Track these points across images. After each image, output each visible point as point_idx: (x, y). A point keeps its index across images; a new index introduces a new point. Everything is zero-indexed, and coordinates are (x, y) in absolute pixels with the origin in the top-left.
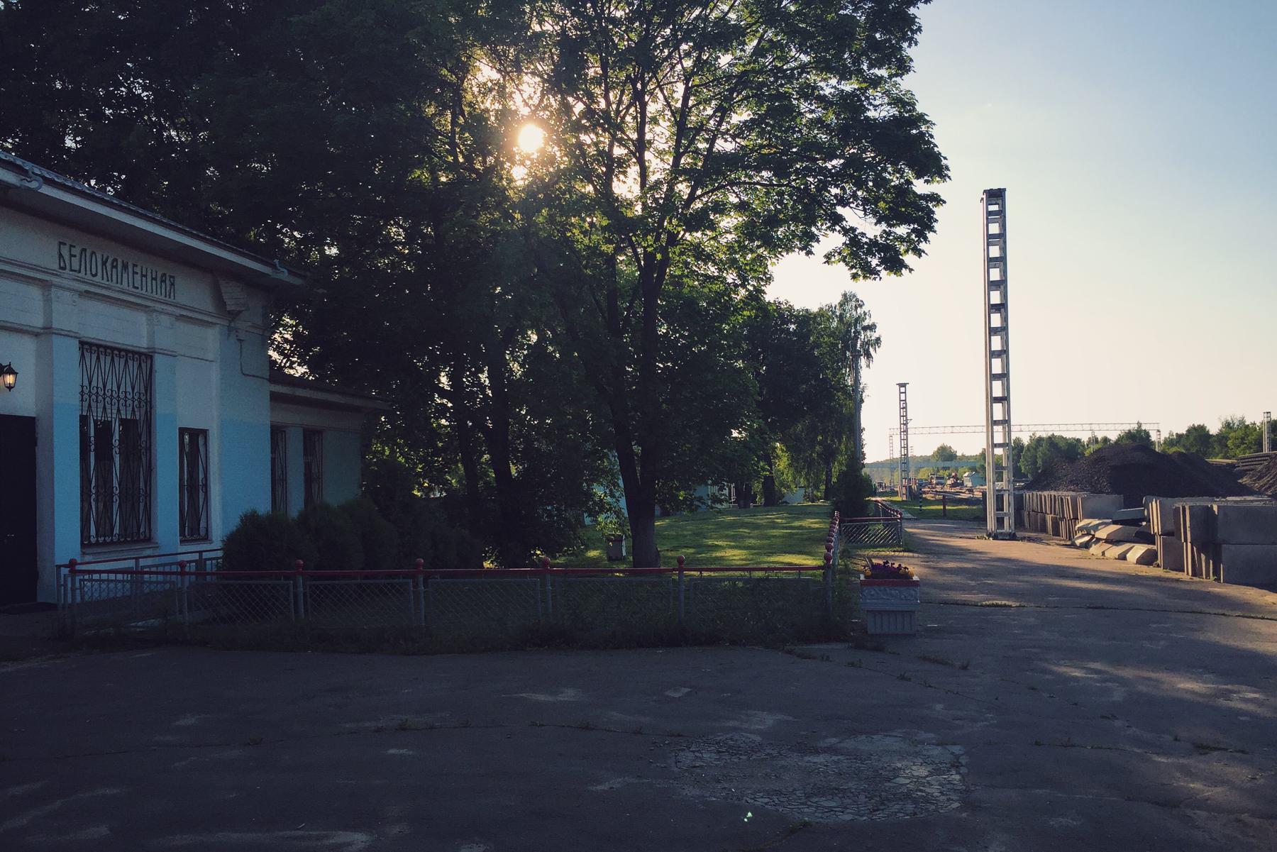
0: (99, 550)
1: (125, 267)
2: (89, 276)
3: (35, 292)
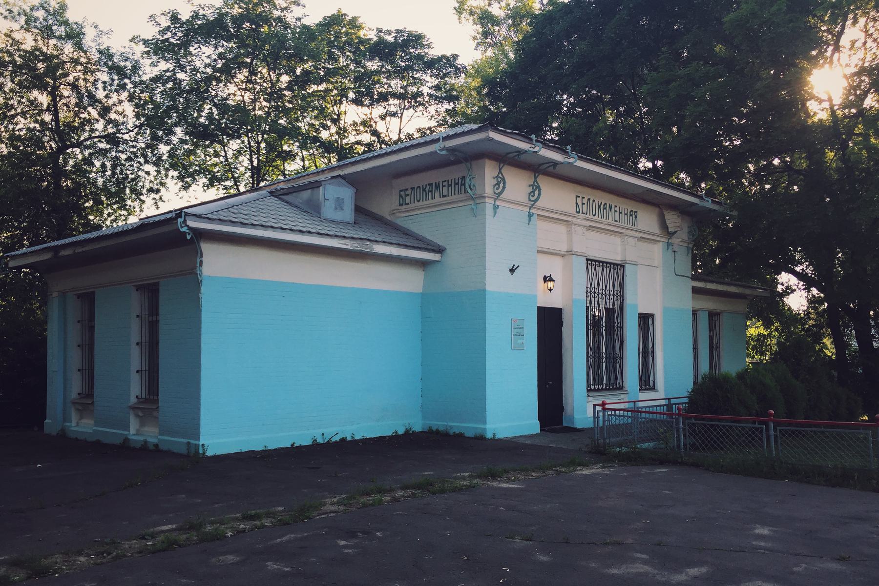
0: (598, 394)
1: (610, 208)
2: (591, 216)
3: (562, 229)
